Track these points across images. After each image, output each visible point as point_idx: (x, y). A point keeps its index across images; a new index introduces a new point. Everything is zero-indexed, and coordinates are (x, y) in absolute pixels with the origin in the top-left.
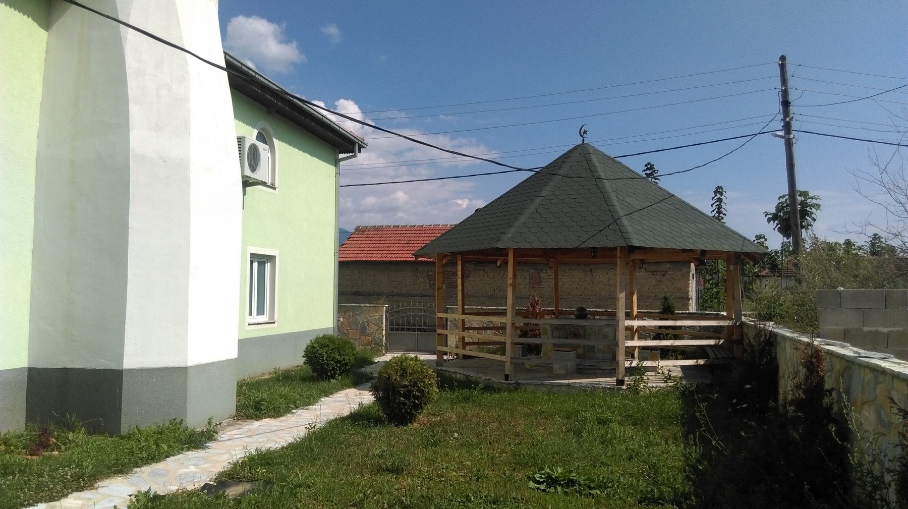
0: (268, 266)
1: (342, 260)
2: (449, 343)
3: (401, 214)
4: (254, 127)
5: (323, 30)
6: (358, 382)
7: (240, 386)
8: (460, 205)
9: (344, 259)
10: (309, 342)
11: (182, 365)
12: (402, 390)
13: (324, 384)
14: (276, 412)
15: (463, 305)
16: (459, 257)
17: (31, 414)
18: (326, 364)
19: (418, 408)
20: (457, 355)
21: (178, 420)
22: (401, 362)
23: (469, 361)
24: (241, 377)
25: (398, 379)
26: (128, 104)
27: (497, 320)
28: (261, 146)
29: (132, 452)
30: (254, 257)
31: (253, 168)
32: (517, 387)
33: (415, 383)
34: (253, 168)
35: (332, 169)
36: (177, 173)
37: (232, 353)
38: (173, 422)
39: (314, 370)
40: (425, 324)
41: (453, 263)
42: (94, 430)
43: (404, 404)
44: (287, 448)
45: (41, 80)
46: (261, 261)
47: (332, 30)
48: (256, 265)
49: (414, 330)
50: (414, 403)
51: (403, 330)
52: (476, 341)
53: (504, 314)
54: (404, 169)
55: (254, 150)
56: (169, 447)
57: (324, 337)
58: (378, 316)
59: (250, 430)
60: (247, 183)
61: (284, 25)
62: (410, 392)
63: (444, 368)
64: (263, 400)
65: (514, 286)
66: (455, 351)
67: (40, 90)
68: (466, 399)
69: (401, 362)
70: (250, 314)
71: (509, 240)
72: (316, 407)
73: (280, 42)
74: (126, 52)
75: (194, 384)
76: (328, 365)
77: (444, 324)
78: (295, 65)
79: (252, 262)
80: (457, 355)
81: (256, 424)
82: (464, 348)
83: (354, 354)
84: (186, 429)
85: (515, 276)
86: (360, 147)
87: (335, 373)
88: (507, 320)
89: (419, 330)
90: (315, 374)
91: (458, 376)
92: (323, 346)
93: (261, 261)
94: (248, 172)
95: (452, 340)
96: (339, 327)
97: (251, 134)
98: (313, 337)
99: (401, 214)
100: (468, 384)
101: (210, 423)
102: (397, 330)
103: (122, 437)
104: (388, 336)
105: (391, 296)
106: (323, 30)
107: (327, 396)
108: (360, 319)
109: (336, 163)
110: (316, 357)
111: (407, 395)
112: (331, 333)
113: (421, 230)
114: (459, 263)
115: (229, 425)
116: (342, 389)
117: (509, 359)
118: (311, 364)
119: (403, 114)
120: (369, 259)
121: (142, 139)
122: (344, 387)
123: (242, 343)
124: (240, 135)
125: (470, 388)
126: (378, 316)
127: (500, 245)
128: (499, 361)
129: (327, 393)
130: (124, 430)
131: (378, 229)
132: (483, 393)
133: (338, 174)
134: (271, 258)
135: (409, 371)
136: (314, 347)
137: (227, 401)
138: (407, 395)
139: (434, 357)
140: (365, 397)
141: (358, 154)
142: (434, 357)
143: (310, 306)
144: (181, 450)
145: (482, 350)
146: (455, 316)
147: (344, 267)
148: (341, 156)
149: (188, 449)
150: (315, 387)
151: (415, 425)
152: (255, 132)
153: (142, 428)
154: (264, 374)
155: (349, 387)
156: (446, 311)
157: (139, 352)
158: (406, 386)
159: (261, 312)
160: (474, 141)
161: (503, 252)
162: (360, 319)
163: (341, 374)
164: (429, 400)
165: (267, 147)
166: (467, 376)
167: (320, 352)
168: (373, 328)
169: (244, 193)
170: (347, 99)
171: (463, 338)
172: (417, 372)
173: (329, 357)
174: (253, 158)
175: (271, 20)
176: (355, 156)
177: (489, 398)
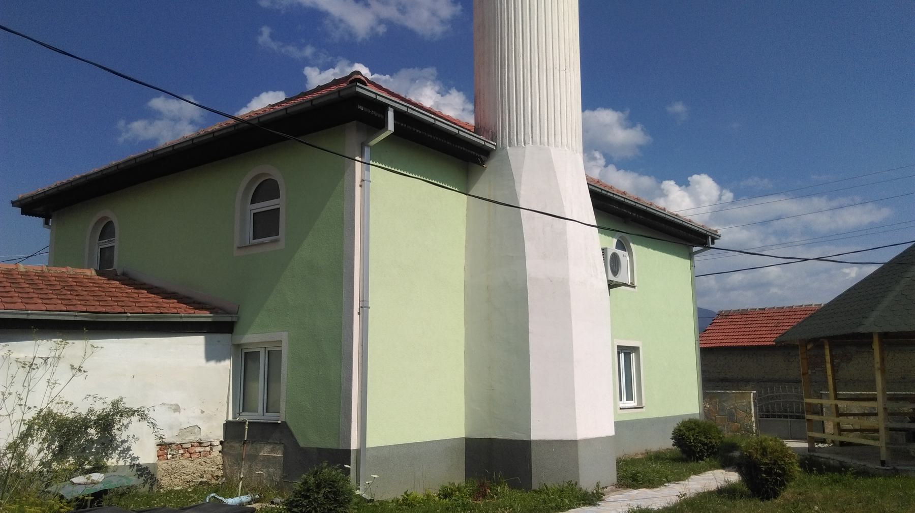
0: (633, 356)
1: (703, 346)
2: (826, 431)
3: (774, 290)
4: (613, 237)
5: (669, 109)
6: (726, 464)
7: (618, 462)
8: (848, 274)
9: (705, 346)
10: (676, 426)
11: (573, 438)
12: (763, 468)
13: (693, 465)
14: (651, 484)
15: (835, 390)
16: (826, 342)
17: (470, 472)
18: (693, 445)
19: (782, 484)
20: (833, 442)
21: (573, 483)
22: (761, 442)
23: (845, 448)
24: (620, 454)
25: (759, 457)
27: (867, 405)
28: (620, 253)
29: (544, 502)
30: (621, 349)
32: (896, 472)
33: (775, 463)
36: (561, 289)
37: (610, 431)
38: (570, 483)
39: (683, 452)
40: (786, 411)
41: (822, 347)
42: (514, 485)
43: (767, 480)
46: (626, 352)
47: (679, 107)
48: (622, 355)
49: (786, 417)
50: (776, 480)
51: (774, 416)
52: (857, 427)
53: (874, 399)
54: (773, 240)
55: (615, 257)
56: (570, 501)
57: (690, 421)
58: (747, 402)
59: (630, 496)
60: (612, 285)
61: (628, 112)
62: (771, 469)
63: (816, 454)
64: (639, 473)
65: (883, 371)
66: (833, 438)
67: (464, 237)
68: (835, 481)
69: (761, 442)
70: (621, 400)
71: (872, 323)
72: (686, 482)
73: (626, 128)
75: (584, 456)
76: (695, 447)
77: (818, 410)
78: (640, 147)
79: (619, 353)
80: (833, 442)
81: (635, 492)
82: (840, 434)
83: (720, 438)
84: (581, 489)
85: (883, 360)
86: (713, 239)
87: (703, 455)
88: (878, 405)
89: (791, 417)
90: (684, 456)
91: (831, 462)
92: (689, 429)
93: (626, 352)
94: (611, 277)
95: (830, 428)
96: (706, 412)
97: (611, 243)
98: (680, 421)
99: (774, 290)
100: (841, 469)
101: (598, 486)
102: (767, 416)
103: (535, 491)
104: (758, 422)
105: (759, 382)
106: (669, 109)
107: (695, 474)
108: (728, 405)
109: (690, 256)
110: (683, 439)
111: (769, 472)
112: (698, 418)
113: (791, 311)
114: (827, 347)
115: (613, 491)
116: (711, 469)
117: (884, 445)
118: (679, 446)
119: (766, 181)
120: (735, 344)
122: (712, 467)
123: (618, 425)
125: (840, 472)
126: (747, 402)
127: (861, 330)
128: (812, 431)
129: (696, 473)
130: (535, 486)
131: (743, 313)
132: (856, 478)
133: (693, 266)
134: (636, 349)
135: (769, 450)
136: (680, 430)
137: (610, 475)
138: (769, 472)
139: (805, 445)
140: (734, 477)
142: (805, 445)
143: (676, 392)
144: (579, 505)
145: (865, 438)
146: (828, 402)
147: (707, 354)
148: (695, 249)
149: (584, 505)
150: (683, 467)
151: (779, 500)
152: (615, 240)
153: (549, 487)
154: (636, 454)
155: (717, 468)
156: (820, 397)
157: (542, 428)
158: (766, 464)
159: (630, 397)
160: (858, 199)
161: (870, 336)
162: (728, 405)
163: (708, 456)
164: (793, 478)
166: (841, 462)
167: (687, 434)
168: (741, 414)
170: (699, 174)
171: (838, 424)
172: (776, 451)
173: (695, 439)
174: (614, 264)
175: (615, 109)
177: (863, 482)
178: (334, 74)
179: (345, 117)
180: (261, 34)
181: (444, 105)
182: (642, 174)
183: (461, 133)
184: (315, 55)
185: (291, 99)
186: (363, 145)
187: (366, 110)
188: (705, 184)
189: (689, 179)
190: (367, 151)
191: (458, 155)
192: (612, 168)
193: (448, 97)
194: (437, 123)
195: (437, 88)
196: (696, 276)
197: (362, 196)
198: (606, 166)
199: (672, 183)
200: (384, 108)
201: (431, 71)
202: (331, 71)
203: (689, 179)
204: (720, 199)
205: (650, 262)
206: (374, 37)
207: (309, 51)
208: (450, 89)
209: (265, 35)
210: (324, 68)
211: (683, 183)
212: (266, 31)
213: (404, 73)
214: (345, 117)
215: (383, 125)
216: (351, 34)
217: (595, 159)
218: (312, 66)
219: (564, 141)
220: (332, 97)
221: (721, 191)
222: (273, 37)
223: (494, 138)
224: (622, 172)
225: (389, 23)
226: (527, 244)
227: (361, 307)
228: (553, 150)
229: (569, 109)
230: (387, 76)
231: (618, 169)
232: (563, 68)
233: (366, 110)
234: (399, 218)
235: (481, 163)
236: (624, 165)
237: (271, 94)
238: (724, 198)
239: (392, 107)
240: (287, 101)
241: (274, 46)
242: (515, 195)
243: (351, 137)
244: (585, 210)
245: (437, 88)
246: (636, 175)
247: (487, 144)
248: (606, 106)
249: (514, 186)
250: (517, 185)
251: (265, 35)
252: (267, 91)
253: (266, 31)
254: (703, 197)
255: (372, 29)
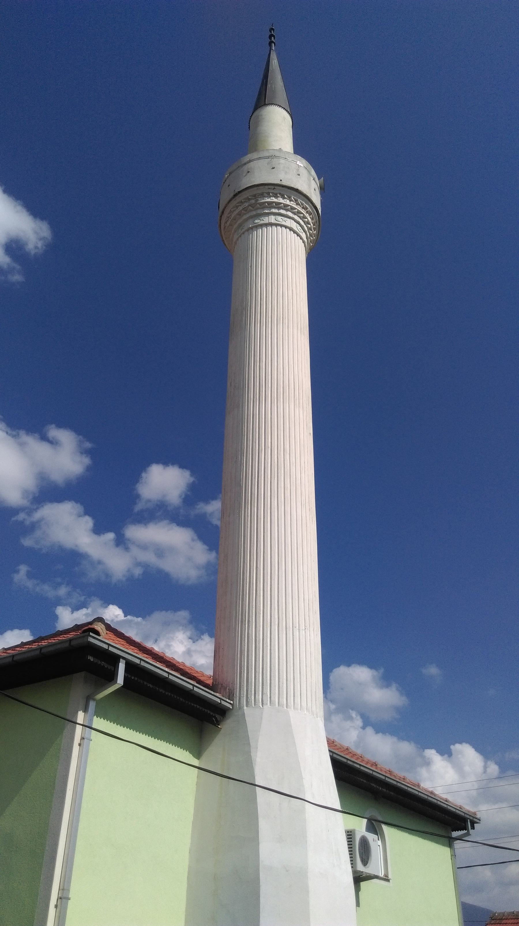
26: (257, 819)
28: (371, 837)
31: (365, 862)
34: (365, 862)
35: (446, 851)
36: (298, 880)
44: (164, 610)
45: (193, 801)
47: (433, 670)
60: (359, 879)
61: (382, 670)
73: (381, 687)
74: (256, 773)
78: (397, 709)
86: (473, 823)
94: (360, 867)
97: (360, 825)
121: (270, 851)
124: (350, 828)
133: (454, 856)
141: (471, 831)
148: (455, 834)
165: (376, 837)
169: (357, 889)
170: (461, 743)
174: (359, 850)
175: (371, 667)
176: (468, 834)
178: (87, 615)
179: (71, 667)
180: (17, 572)
181: (195, 651)
182: (401, 738)
183: (195, 689)
184: (69, 594)
185: (42, 639)
186: (88, 698)
187: (96, 661)
188: (468, 754)
189: (452, 747)
190: (92, 705)
191: (191, 711)
192: (370, 730)
193: (200, 642)
194: (171, 677)
195: (188, 633)
196: (459, 868)
197: (80, 757)
198: (364, 728)
199: (433, 751)
200: (115, 659)
201: (184, 614)
202: (84, 611)
203: (452, 747)
204: (485, 772)
205: (403, 849)
206: (130, 579)
207: (63, 591)
208: (203, 633)
209: (22, 574)
210: (76, 608)
211: (445, 752)
212: (23, 569)
213: (158, 616)
214: (71, 667)
215: (112, 678)
216: (108, 575)
217: (351, 718)
218: (64, 605)
219: (304, 704)
220: (33, 654)
221: (486, 763)
222: (30, 575)
223: (231, 696)
224: (380, 735)
225: (146, 566)
226: (260, 820)
227: (60, 898)
228: (292, 713)
229: (309, 669)
230: (140, 619)
231: (377, 732)
232: (302, 627)
233: (96, 661)
234: (119, 783)
235: (216, 723)
236: (381, 728)
237: (16, 632)
238: (489, 770)
239: (124, 658)
240: (33, 642)
241: (30, 584)
242: (248, 764)
243: (78, 687)
244: (323, 785)
245: (188, 633)
246: (395, 739)
247: (223, 703)
248: (362, 662)
249: (250, 752)
250: (252, 750)
251: (22, 574)
252: (12, 629)
253: (23, 569)
254: (467, 769)
255: (129, 570)
